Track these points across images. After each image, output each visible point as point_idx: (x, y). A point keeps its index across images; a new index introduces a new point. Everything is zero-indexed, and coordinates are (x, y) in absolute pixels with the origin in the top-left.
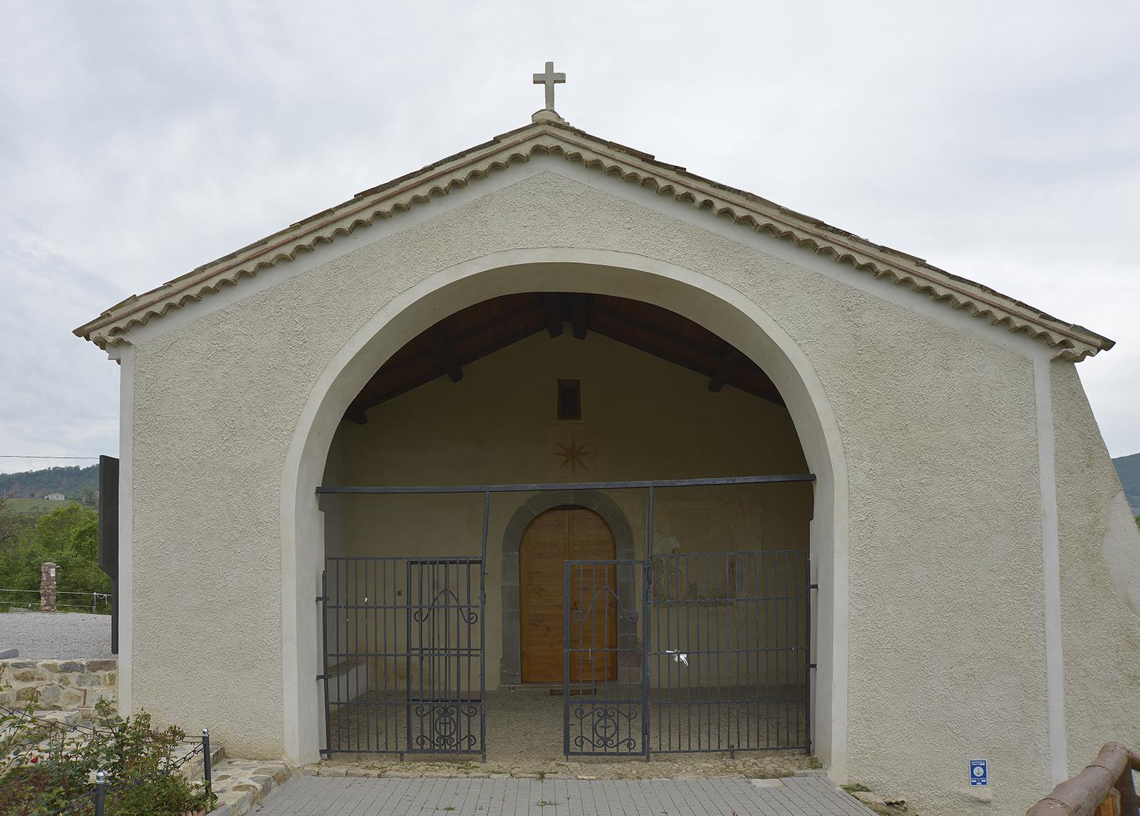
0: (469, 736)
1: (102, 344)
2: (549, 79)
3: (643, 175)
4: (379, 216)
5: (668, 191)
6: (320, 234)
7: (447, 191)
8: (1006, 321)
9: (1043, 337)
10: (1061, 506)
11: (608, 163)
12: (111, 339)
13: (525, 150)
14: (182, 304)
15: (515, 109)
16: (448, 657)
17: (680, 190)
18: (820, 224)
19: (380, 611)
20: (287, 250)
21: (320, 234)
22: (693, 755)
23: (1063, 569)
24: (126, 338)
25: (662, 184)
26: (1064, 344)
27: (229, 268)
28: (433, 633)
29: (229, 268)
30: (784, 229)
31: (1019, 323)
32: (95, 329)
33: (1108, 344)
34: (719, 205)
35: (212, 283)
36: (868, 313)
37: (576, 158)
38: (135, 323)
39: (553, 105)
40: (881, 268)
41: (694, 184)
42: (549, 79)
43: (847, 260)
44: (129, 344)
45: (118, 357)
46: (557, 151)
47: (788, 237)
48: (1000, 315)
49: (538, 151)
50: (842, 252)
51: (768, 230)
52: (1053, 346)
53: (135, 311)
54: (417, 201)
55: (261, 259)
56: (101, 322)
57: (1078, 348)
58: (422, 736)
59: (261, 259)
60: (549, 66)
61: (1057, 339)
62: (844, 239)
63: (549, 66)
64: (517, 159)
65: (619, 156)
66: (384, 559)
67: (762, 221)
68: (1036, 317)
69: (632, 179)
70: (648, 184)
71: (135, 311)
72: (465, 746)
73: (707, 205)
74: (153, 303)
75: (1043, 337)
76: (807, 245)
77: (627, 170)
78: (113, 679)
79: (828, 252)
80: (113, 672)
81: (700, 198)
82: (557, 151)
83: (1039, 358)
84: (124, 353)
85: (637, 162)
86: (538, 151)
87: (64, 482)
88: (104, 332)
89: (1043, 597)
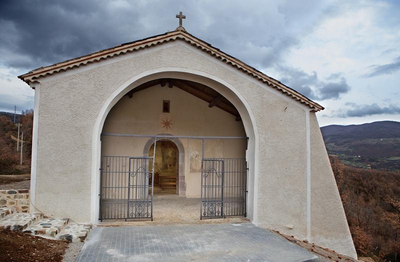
0: (147, 213)
1: (28, 82)
2: (181, 17)
3: (208, 50)
4: (135, 50)
5: (214, 55)
6: (109, 55)
7: (150, 47)
8: (300, 100)
9: (308, 105)
10: (311, 150)
11: (198, 45)
12: (33, 81)
13: (174, 38)
14: (60, 71)
15: (174, 25)
16: (213, 188)
17: (218, 55)
18: (254, 69)
19: (124, 174)
20: (98, 59)
21: (109, 55)
22: (119, 220)
23: (311, 167)
24: (39, 81)
25: (213, 53)
26: (313, 108)
27: (78, 62)
28: (145, 181)
29: (78, 62)
30: (245, 70)
31: (303, 101)
32: (26, 77)
33: (323, 109)
34: (228, 61)
35: (71, 66)
36: (265, 95)
37: (189, 42)
38: (41, 76)
39: (181, 24)
40: (270, 83)
41: (222, 54)
42: (181, 17)
43: (261, 80)
44: (39, 83)
45: (34, 87)
46: (183, 39)
47: (246, 72)
48: (298, 98)
49: (178, 38)
50: (260, 77)
51: (241, 69)
52: (310, 108)
53: (42, 72)
54: (141, 48)
55: (89, 60)
56: (29, 74)
57: (316, 109)
58: (205, 212)
59: (89, 60)
60: (181, 13)
61: (312, 106)
62: (260, 74)
63: (181, 13)
64: (171, 40)
65: (201, 43)
66: (120, 157)
67: (239, 67)
68: (307, 100)
69: (204, 50)
70: (209, 52)
71: (42, 72)
72: (217, 214)
73: (225, 61)
74: (49, 70)
75: (308, 105)
76: (251, 75)
77: (203, 48)
78: (28, 196)
79: (256, 77)
80: (27, 194)
81: (223, 58)
82: (183, 39)
83: (307, 110)
84: (36, 86)
85: (206, 46)
86: (178, 38)
87: (302, 131)
88: (30, 78)
89: (306, 174)
